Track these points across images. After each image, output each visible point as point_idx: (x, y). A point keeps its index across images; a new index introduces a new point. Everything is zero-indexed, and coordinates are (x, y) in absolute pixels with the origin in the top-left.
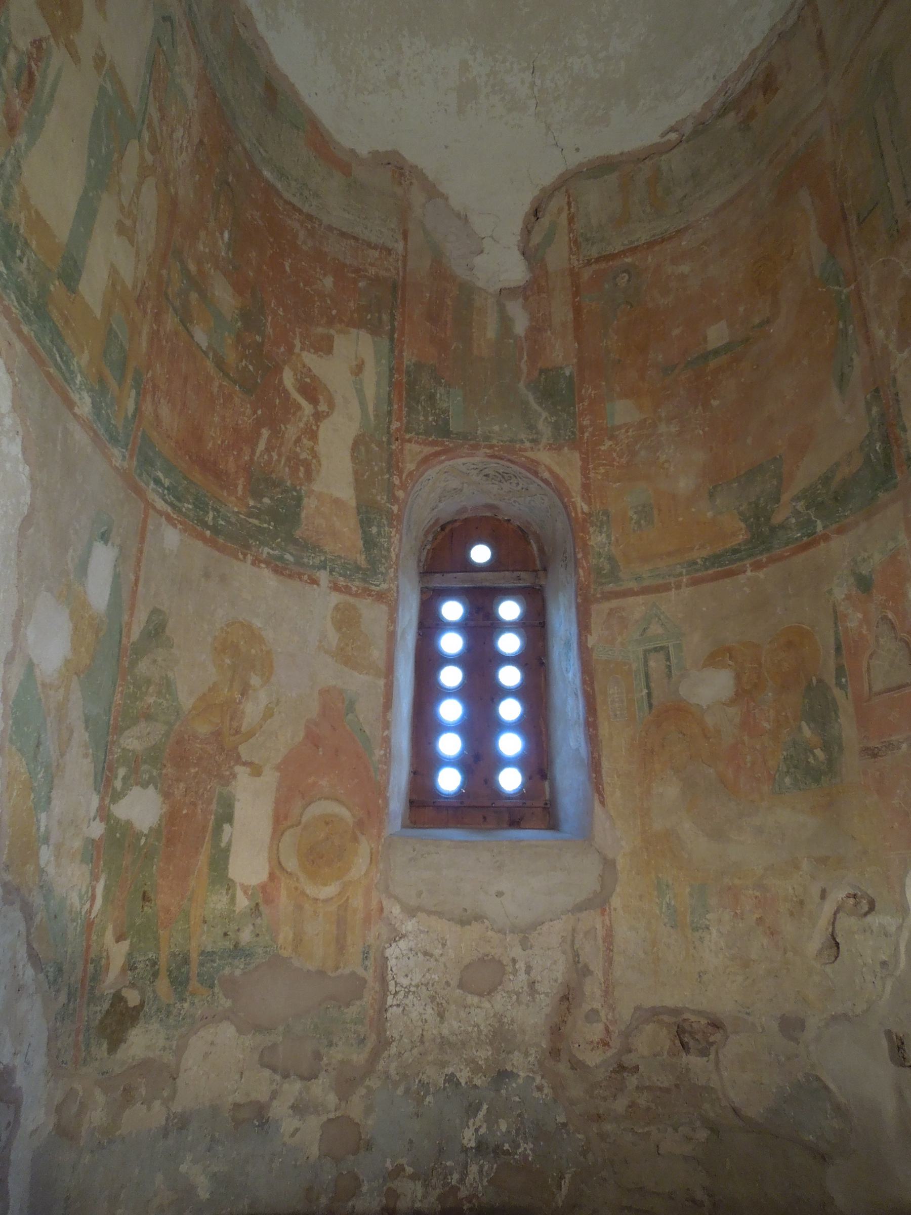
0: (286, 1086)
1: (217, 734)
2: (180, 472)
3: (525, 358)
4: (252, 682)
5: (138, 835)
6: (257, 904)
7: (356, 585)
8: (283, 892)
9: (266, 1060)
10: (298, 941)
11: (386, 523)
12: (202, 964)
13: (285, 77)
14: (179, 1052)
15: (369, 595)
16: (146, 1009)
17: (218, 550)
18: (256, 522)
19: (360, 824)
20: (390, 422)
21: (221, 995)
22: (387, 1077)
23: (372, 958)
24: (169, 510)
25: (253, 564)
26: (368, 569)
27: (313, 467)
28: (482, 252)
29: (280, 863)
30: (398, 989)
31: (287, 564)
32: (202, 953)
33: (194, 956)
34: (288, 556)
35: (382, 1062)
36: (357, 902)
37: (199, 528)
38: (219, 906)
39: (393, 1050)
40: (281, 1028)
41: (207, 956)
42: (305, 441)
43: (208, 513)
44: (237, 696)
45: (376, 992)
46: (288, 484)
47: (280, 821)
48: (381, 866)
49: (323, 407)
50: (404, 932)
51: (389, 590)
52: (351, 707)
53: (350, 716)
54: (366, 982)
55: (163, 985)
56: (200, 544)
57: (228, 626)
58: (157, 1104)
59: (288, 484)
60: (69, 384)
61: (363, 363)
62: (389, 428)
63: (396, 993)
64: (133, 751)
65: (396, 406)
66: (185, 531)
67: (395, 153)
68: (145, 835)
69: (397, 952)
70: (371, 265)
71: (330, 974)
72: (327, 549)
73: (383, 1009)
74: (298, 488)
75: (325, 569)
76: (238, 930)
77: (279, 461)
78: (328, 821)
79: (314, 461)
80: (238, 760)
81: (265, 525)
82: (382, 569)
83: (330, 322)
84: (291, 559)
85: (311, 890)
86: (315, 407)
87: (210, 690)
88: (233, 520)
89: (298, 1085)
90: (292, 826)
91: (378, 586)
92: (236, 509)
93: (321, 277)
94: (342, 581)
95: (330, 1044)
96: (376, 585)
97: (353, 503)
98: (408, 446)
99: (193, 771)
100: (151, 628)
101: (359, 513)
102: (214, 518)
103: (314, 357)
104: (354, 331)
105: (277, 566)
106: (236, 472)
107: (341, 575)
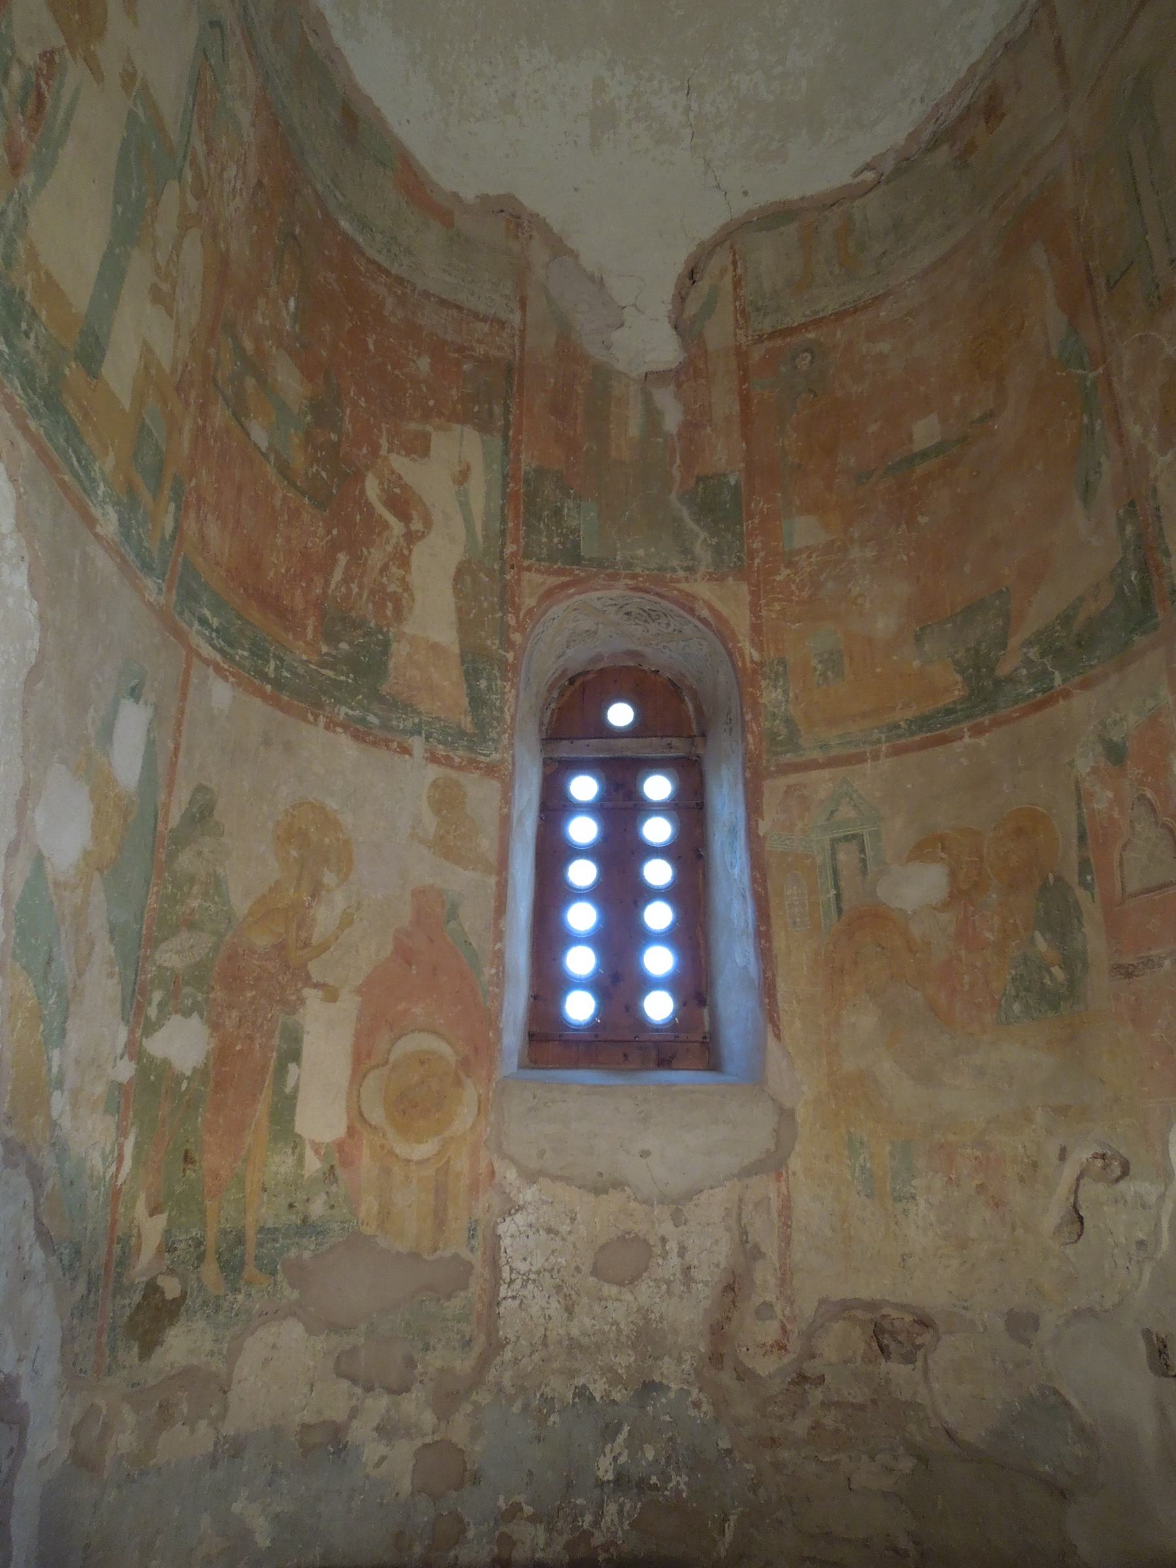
0: (369, 1402)
1: (281, 947)
2: (233, 609)
3: (678, 461)
4: (326, 880)
5: (178, 1078)
6: (332, 1167)
7: (460, 755)
8: (366, 1152)
9: (344, 1368)
10: (385, 1214)
11: (498, 674)
12: (260, 1245)
13: (368, 100)
14: (232, 1357)
15: (477, 768)
16: (189, 1302)
17: (282, 709)
18: (330, 673)
19: (465, 1064)
20: (503, 545)
21: (285, 1284)
22: (500, 1390)
23: (480, 1237)
24: (219, 658)
25: (327, 727)
26: (475, 735)
27: (404, 602)
28: (622, 325)
29: (361, 1114)
30: (513, 1276)
31: (371, 728)
32: (261, 1230)
33: (251, 1234)
34: (371, 718)
35: (493, 1370)
36: (461, 1164)
37: (257, 682)
38: (282, 1170)
39: (508, 1355)
40: (363, 1327)
41: (268, 1234)
42: (394, 569)
43: (268, 662)
44: (306, 898)
45: (486, 1280)
46: (372, 624)
47: (362, 1059)
48: (492, 1118)
49: (417, 525)
50: (521, 1203)
51: (502, 761)
52: (453, 913)
53: (452, 924)
54: (472, 1267)
55: (210, 1271)
56: (258, 702)
57: (294, 807)
58: (203, 1425)
59: (372, 624)
60: (89, 496)
61: (469, 468)
62: (502, 552)
63: (512, 1281)
64: (172, 969)
65: (511, 525)
66: (239, 685)
67: (510, 197)
68: (188, 1078)
69: (513, 1229)
70: (480, 341)
71: (426, 1257)
72: (422, 708)
73: (494, 1302)
74: (385, 630)
75: (420, 734)
76: (308, 1200)
77: (360, 595)
78: (423, 1059)
79: (406, 595)
80: (308, 981)
81: (343, 678)
82: (494, 735)
83: (427, 416)
84: (376, 721)
85: (401, 1149)
86: (407, 526)
87: (271, 890)
88: (301, 671)
89: (384, 1401)
90: (377, 1066)
91: (488, 756)
92: (304, 657)
93: (415, 358)
94: (441, 750)
95: (427, 1348)
96: (485, 755)
97: (456, 649)
98: (526, 576)
99: (249, 995)
100: (194, 810)
101: (463, 662)
102: (276, 668)
103: (406, 460)
104: (457, 427)
105: (357, 730)
106: (305, 609)
107: (440, 742)
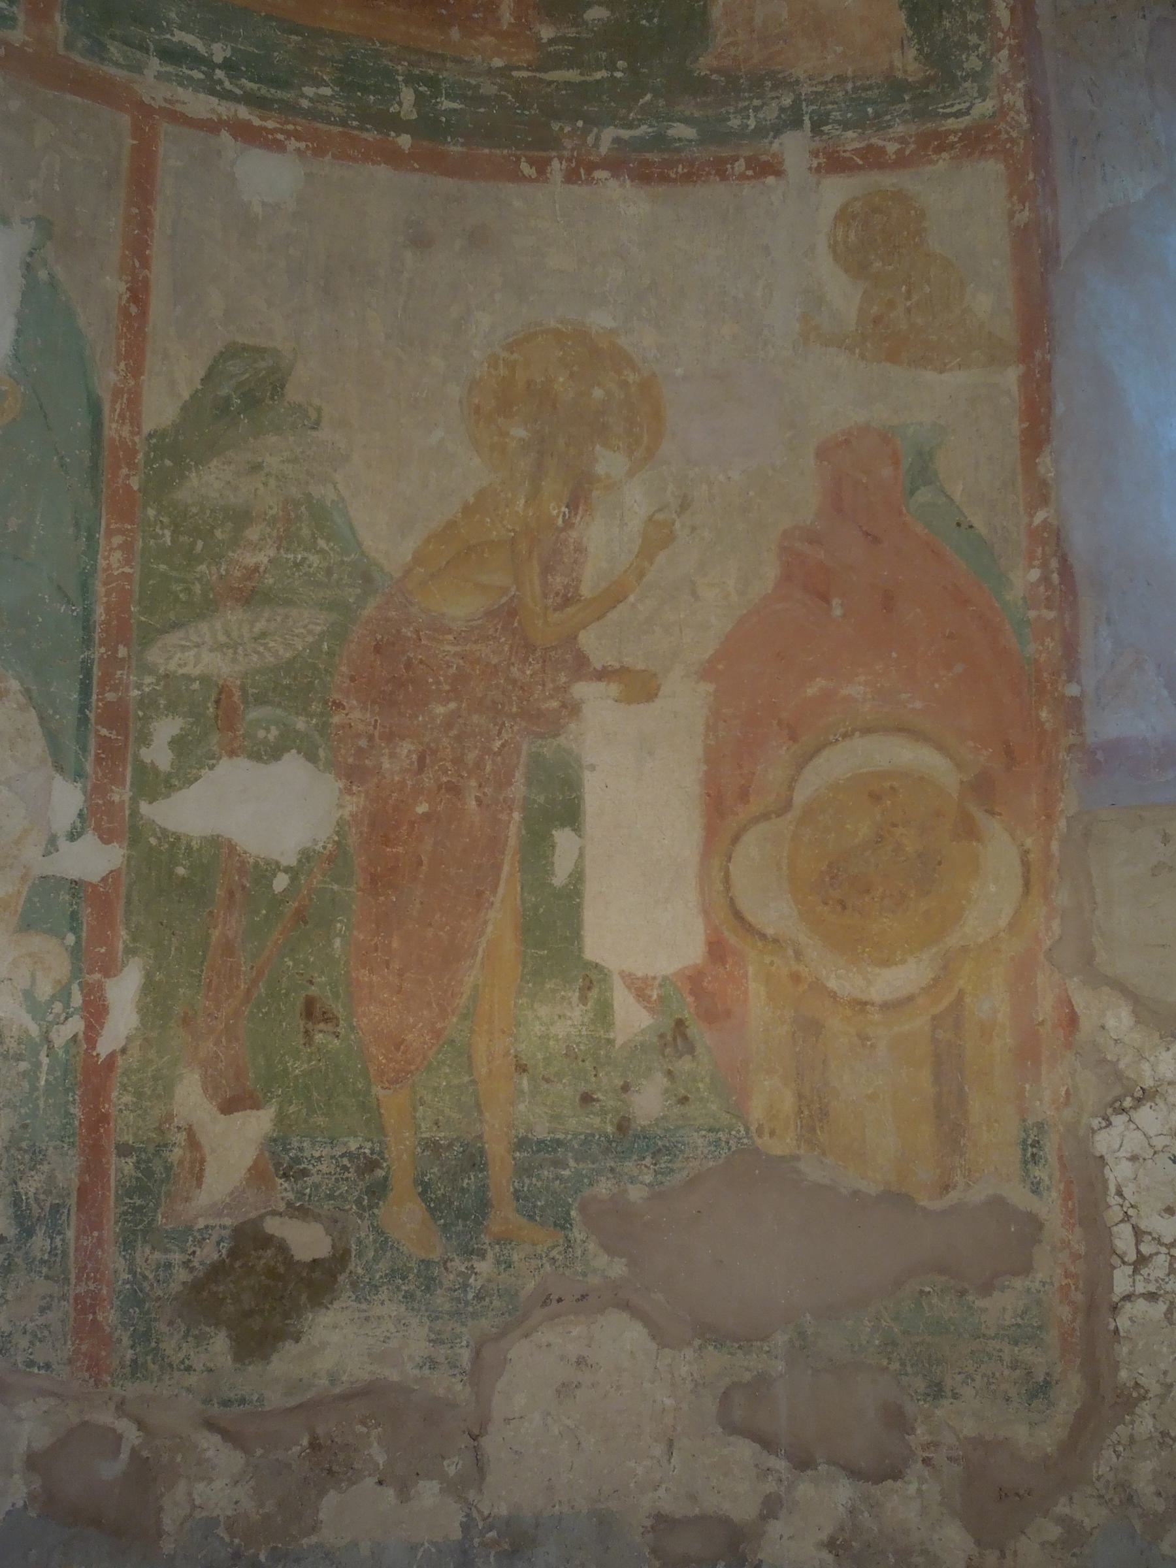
0: (805, 1489)
1: (507, 615)
4: (600, 469)
5: (264, 872)
6: (680, 1023)
7: (901, 130)
8: (756, 989)
9: (740, 1412)
10: (814, 1115)
12: (524, 1170)
14: (481, 1371)
15: (940, 149)
16: (356, 1266)
17: (451, 172)
18: (572, 75)
19: (983, 788)
21: (592, 1246)
22: (1130, 1499)
23: (1053, 1159)
24: (243, 112)
25: (571, 177)
29: (738, 916)
30: (1145, 1249)
31: (678, 150)
32: (522, 1143)
33: (497, 1150)
34: (681, 131)
35: (1108, 1454)
36: (992, 1003)
37: (371, 136)
38: (560, 1030)
39: (1144, 1424)
40: (780, 1339)
41: (535, 1151)
43: (397, 92)
44: (556, 511)
45: (1075, 1257)
47: (724, 809)
48: (1062, 898)
50: (1148, 1083)
51: (1002, 112)
52: (923, 471)
53: (924, 495)
54: (1040, 1226)
55: (405, 1217)
56: (383, 172)
57: (510, 348)
58: (428, 1492)
63: (1142, 1260)
64: (205, 680)
66: (319, 152)
68: (287, 870)
69: (1134, 1142)
71: (924, 1203)
73: (1097, 1305)
75: (797, 124)
76: (625, 1088)
78: (876, 790)
80: (581, 666)
82: (973, 63)
85: (844, 980)
87: (467, 509)
88: (489, 88)
89: (843, 1492)
90: (765, 816)
92: (498, 63)
94: (851, 140)
95: (936, 1391)
99: (440, 710)
100: (224, 391)
102: (420, 98)
103: (631, 999)
105: (648, 164)
107: (846, 125)
